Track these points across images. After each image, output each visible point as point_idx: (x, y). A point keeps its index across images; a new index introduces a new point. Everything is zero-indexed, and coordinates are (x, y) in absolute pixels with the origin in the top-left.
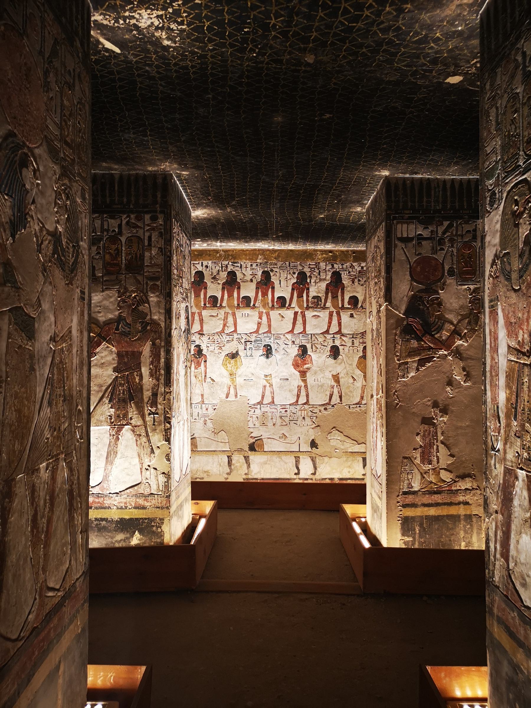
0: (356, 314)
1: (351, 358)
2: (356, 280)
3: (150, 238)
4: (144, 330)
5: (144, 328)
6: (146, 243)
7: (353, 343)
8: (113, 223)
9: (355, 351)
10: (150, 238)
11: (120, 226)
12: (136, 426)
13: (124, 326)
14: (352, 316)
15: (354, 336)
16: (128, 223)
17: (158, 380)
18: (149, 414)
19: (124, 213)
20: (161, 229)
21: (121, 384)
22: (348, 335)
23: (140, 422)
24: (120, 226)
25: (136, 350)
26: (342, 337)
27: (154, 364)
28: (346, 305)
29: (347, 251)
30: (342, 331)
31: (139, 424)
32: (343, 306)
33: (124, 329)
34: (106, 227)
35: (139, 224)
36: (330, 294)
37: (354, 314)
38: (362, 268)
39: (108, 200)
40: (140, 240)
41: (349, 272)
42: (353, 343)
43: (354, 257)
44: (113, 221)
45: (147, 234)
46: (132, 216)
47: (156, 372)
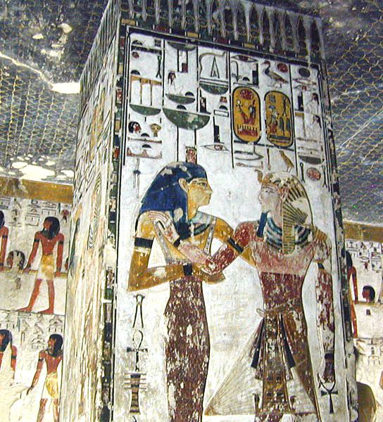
0: (374, 312)
1: (372, 374)
2: (370, 265)
3: (300, 99)
4: (303, 241)
5: (303, 238)
6: (296, 105)
7: (373, 352)
8: (246, 69)
9: (377, 363)
10: (300, 99)
11: (255, 74)
12: (301, 414)
13: (270, 230)
14: (368, 313)
15: (374, 342)
16: (267, 72)
17: (332, 328)
18: (323, 393)
19: (261, 56)
20: (314, 90)
21: (271, 334)
22: (366, 340)
23: (308, 407)
24: (255, 74)
25: (292, 273)
26: (359, 342)
27: (325, 301)
28: (361, 298)
29: (356, 225)
30: (358, 333)
31: (307, 410)
32: (356, 298)
33: (271, 234)
34: (233, 71)
35: (283, 76)
36: (45, 365)
37: (371, 311)
38: (375, 249)
39: (236, 35)
40: (286, 100)
41: (360, 254)
42: (373, 352)
43: (364, 233)
44: (244, 64)
45: (296, 93)
46: (273, 63)
47: (328, 316)
